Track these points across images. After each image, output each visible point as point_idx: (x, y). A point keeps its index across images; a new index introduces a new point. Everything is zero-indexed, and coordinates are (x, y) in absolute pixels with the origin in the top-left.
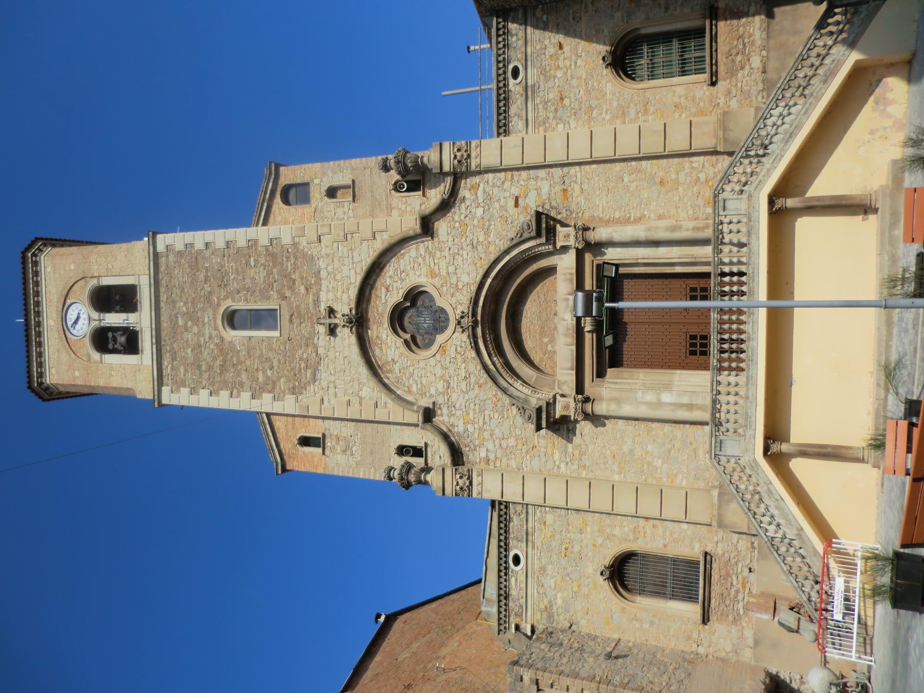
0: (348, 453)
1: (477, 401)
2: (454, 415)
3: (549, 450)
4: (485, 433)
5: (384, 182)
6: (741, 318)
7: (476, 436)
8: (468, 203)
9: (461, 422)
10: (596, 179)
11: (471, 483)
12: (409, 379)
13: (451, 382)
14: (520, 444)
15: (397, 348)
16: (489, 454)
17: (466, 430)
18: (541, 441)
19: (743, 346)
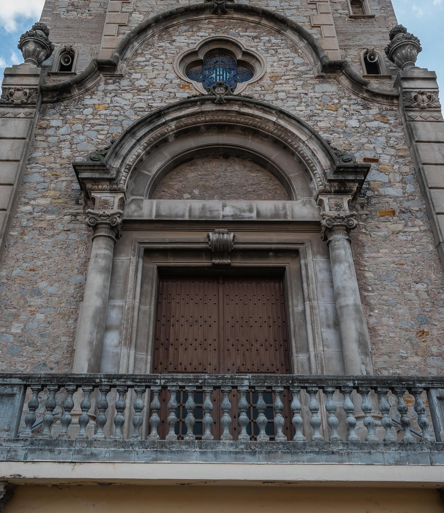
0: (70, 8)
1: (120, 118)
2: (106, 95)
3: (52, 193)
4: (81, 126)
5: (374, 43)
6: (244, 431)
7: (78, 116)
8: (363, 112)
9: (96, 102)
10: (414, 250)
11: (17, 106)
12: (151, 54)
13: (146, 93)
14: (63, 161)
15: (188, 44)
16: (53, 129)
17: (86, 107)
18: (64, 184)
19: (190, 436)
